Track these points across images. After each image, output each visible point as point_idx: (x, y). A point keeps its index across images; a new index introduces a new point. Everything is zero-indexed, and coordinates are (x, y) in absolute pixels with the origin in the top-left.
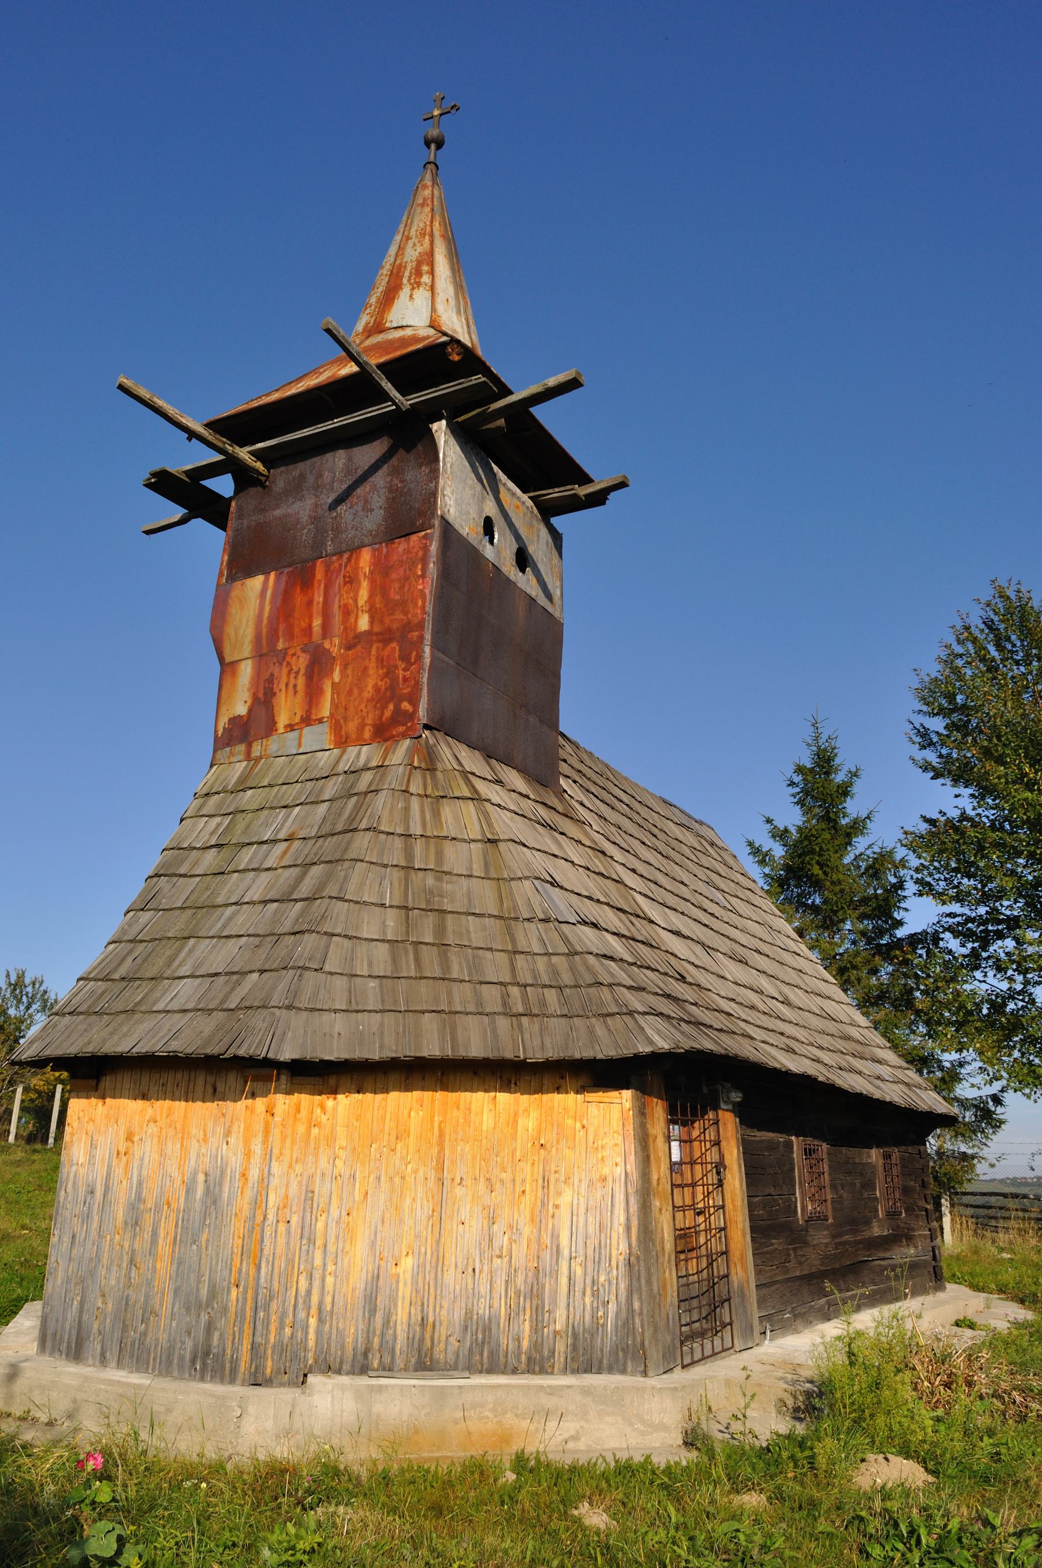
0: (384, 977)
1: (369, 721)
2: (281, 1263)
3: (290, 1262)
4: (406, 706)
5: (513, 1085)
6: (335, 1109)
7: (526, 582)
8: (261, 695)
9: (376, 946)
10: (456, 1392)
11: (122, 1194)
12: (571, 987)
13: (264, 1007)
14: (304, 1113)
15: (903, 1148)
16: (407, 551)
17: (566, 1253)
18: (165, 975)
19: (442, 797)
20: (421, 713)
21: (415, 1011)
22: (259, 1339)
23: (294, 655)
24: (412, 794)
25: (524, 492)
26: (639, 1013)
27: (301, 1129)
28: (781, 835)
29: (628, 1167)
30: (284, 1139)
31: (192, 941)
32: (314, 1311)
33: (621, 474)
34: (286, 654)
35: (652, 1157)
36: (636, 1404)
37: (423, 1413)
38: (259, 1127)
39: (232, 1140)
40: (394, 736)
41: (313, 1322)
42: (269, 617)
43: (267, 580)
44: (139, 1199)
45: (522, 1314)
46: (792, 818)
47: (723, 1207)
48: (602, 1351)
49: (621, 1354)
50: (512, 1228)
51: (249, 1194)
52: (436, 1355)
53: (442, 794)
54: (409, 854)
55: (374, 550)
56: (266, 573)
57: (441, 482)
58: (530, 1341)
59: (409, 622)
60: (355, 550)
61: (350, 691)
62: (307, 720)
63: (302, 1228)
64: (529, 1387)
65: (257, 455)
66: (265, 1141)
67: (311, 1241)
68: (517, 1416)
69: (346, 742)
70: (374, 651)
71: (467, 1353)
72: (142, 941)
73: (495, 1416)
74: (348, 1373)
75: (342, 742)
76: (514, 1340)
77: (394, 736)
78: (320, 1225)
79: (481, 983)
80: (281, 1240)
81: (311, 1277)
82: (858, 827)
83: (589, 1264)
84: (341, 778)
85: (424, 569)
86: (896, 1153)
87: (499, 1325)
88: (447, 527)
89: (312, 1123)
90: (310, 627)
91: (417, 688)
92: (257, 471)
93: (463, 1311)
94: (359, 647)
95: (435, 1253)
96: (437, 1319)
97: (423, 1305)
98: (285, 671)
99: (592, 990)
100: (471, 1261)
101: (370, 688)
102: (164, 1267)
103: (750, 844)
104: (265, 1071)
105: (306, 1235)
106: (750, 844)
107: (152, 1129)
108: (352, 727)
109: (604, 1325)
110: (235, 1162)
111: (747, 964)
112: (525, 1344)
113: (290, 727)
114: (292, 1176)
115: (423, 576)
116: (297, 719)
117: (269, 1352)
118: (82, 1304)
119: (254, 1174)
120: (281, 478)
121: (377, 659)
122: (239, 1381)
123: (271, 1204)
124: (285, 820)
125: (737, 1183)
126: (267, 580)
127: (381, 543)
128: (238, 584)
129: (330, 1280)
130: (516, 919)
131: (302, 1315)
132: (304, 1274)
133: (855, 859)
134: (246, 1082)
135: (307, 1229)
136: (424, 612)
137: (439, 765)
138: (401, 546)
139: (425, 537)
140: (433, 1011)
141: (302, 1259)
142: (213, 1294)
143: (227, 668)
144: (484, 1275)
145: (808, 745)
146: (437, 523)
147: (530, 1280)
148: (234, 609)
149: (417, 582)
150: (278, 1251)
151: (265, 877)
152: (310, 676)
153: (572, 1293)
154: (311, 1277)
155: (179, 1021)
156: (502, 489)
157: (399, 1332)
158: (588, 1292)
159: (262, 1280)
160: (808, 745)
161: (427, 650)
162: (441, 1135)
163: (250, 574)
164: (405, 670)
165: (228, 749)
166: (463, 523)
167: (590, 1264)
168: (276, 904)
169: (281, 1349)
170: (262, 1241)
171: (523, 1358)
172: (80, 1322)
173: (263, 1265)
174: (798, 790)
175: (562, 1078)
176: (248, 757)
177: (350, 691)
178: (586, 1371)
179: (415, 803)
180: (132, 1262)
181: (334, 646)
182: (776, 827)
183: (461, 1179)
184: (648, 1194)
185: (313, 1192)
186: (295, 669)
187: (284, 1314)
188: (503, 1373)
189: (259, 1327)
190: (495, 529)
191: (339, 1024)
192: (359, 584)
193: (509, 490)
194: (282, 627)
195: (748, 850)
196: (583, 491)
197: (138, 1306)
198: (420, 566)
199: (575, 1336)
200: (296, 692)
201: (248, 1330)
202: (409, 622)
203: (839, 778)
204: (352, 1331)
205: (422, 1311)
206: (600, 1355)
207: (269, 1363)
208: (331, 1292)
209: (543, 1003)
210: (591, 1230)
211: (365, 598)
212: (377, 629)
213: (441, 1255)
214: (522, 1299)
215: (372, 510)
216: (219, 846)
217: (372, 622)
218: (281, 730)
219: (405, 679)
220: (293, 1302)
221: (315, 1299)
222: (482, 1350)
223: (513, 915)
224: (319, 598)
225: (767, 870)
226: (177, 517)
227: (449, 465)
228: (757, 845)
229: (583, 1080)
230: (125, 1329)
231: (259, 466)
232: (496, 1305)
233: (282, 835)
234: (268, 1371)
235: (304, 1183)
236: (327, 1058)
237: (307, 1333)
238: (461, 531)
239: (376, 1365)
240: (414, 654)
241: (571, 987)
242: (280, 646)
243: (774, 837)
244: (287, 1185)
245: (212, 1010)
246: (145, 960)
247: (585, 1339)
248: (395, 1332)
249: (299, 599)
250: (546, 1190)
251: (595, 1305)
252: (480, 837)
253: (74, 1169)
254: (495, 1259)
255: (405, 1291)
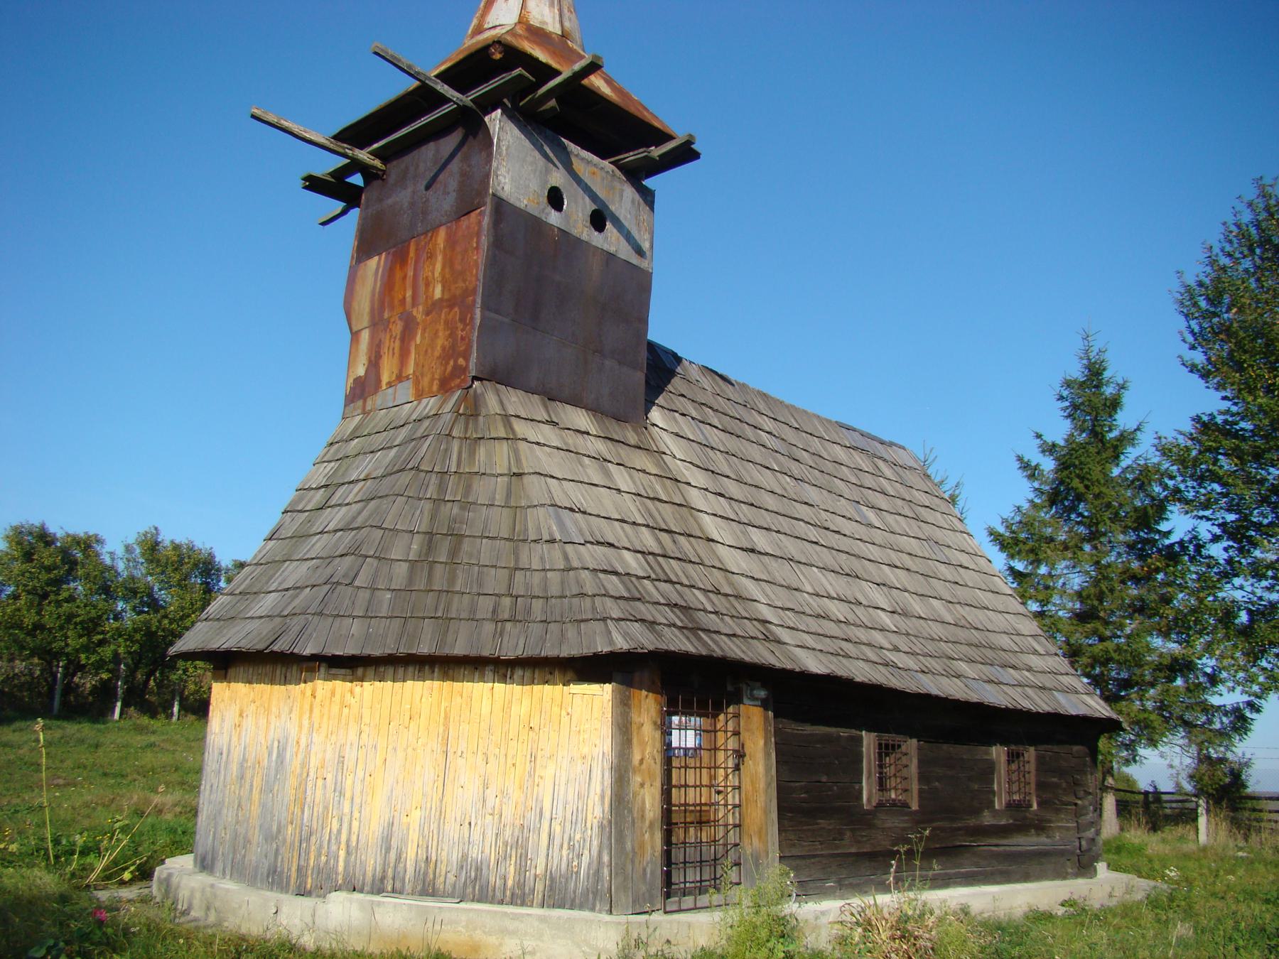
0: (399, 590)
1: (437, 376)
2: (319, 809)
3: (326, 808)
4: (461, 361)
5: (508, 679)
6: (362, 694)
7: (609, 240)
8: (373, 359)
9: (400, 566)
10: (437, 911)
11: (236, 756)
12: (556, 597)
13: (304, 614)
14: (338, 696)
15: (1041, 747)
16: (468, 228)
17: (547, 815)
18: (263, 591)
19: (480, 438)
20: (471, 367)
21: (417, 617)
22: (302, 863)
23: (394, 322)
24: (453, 437)
25: (603, 158)
26: (612, 619)
27: (335, 709)
28: (1050, 449)
29: (605, 747)
30: (322, 716)
31: (288, 562)
32: (343, 846)
33: (686, 134)
34: (389, 322)
35: (635, 741)
36: (584, 932)
37: (410, 924)
38: (307, 707)
39: (293, 716)
40: (452, 388)
41: (342, 853)
42: (379, 292)
43: (380, 259)
44: (245, 760)
45: (508, 859)
46: (1059, 429)
47: (739, 788)
48: (575, 892)
49: (591, 896)
50: (503, 793)
51: (300, 756)
52: (437, 885)
53: (479, 436)
54: (442, 488)
55: (448, 228)
56: (380, 254)
57: (494, 164)
58: (514, 881)
59: (467, 289)
60: (435, 229)
61: (426, 351)
62: (400, 378)
63: (336, 784)
64: (496, 912)
65: (375, 154)
66: (310, 717)
67: (342, 794)
68: (484, 932)
69: (422, 395)
70: (443, 315)
71: (462, 885)
72: (262, 564)
73: (467, 931)
74: (368, 893)
75: (420, 395)
76: (500, 879)
77: (452, 388)
78: (349, 782)
79: (479, 594)
80: (319, 793)
81: (341, 820)
82: (1127, 438)
83: (567, 824)
84: (411, 425)
85: (478, 243)
86: (1031, 753)
87: (489, 866)
88: (501, 206)
89: (343, 705)
90: (404, 298)
91: (469, 347)
92: (375, 167)
93: (460, 855)
94: (434, 313)
95: (438, 809)
96: (439, 859)
97: (427, 847)
98: (388, 337)
99: (575, 601)
100: (467, 816)
101: (439, 348)
102: (255, 810)
103: (1020, 459)
104: (311, 664)
105: (338, 789)
106: (1020, 459)
107: (253, 707)
108: (425, 382)
109: (578, 873)
110: (293, 732)
111: (858, 577)
112: (510, 883)
113: (390, 385)
114: (328, 745)
115: (477, 248)
116: (394, 377)
117: (310, 872)
118: (214, 833)
119: (303, 742)
120: (396, 168)
121: (445, 322)
122: (290, 891)
123: (312, 765)
124: (370, 461)
125: (761, 769)
126: (380, 259)
127: (451, 221)
128: (362, 264)
129: (355, 824)
130: (524, 541)
131: (334, 848)
132: (336, 818)
133: (1122, 472)
134: (302, 673)
135: (339, 784)
136: (477, 279)
137: (483, 412)
138: (465, 222)
139: (480, 214)
140: (432, 618)
141: (335, 807)
142: (279, 831)
143: (355, 335)
144: (479, 827)
145: (1081, 358)
146: (489, 200)
147: (516, 834)
148: (358, 287)
149: (473, 253)
150: (317, 800)
151: (344, 509)
152: (403, 340)
153: (551, 846)
154: (341, 820)
155: (257, 623)
156: (574, 160)
157: (408, 866)
158: (565, 846)
159: (305, 820)
160: (1081, 358)
161: (478, 312)
162: (447, 717)
163: (370, 257)
164: (462, 330)
165: (352, 405)
166: (521, 197)
167: (568, 825)
168: (341, 532)
169: (319, 871)
170: (306, 792)
171: (508, 893)
172: (213, 848)
173: (306, 809)
174: (1067, 404)
175: (551, 673)
176: (364, 412)
177: (426, 351)
178: (559, 907)
179: (455, 446)
180: (239, 805)
181: (418, 313)
182: (1045, 441)
183: (462, 752)
184: (626, 771)
185: (344, 757)
186: (394, 334)
187: (321, 846)
188: (491, 903)
189: (303, 854)
190: (565, 197)
191: (356, 627)
192: (436, 258)
193: (583, 159)
194: (387, 300)
195: (1017, 465)
196: (656, 152)
197: (242, 836)
198: (475, 240)
199: (552, 879)
200: (394, 354)
201: (296, 855)
202: (467, 289)
203: (1109, 391)
204: (372, 862)
205: (427, 852)
206: (572, 896)
207: (309, 881)
208: (356, 833)
209: (529, 611)
210: (570, 798)
211: (439, 270)
212: (446, 297)
213: (443, 811)
214: (509, 848)
215: (449, 193)
216: (326, 486)
217: (443, 291)
218: (384, 387)
219: (463, 339)
220: (327, 838)
221: (344, 837)
222: (475, 885)
223: (521, 538)
224: (410, 273)
225: (1036, 484)
226: (338, 211)
227: (504, 148)
228: (1026, 460)
229: (570, 675)
230: (234, 853)
231: (377, 163)
232: (487, 851)
233: (361, 477)
234: (309, 886)
235: (338, 750)
236: (337, 653)
237: (338, 862)
238: (517, 204)
239: (389, 888)
240: (469, 316)
241: (556, 597)
242: (386, 315)
243: (1043, 452)
244: (325, 751)
245: (274, 616)
246: (257, 579)
247: (561, 883)
248: (405, 866)
249: (398, 275)
250: (533, 763)
251: (571, 856)
252: (506, 472)
253: (213, 736)
254: (487, 816)
255: (414, 836)
